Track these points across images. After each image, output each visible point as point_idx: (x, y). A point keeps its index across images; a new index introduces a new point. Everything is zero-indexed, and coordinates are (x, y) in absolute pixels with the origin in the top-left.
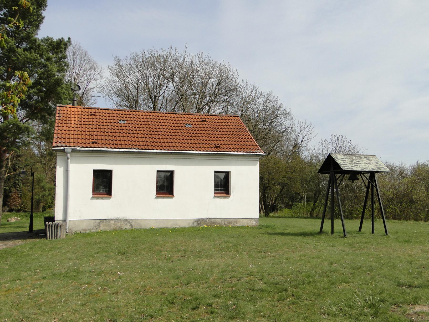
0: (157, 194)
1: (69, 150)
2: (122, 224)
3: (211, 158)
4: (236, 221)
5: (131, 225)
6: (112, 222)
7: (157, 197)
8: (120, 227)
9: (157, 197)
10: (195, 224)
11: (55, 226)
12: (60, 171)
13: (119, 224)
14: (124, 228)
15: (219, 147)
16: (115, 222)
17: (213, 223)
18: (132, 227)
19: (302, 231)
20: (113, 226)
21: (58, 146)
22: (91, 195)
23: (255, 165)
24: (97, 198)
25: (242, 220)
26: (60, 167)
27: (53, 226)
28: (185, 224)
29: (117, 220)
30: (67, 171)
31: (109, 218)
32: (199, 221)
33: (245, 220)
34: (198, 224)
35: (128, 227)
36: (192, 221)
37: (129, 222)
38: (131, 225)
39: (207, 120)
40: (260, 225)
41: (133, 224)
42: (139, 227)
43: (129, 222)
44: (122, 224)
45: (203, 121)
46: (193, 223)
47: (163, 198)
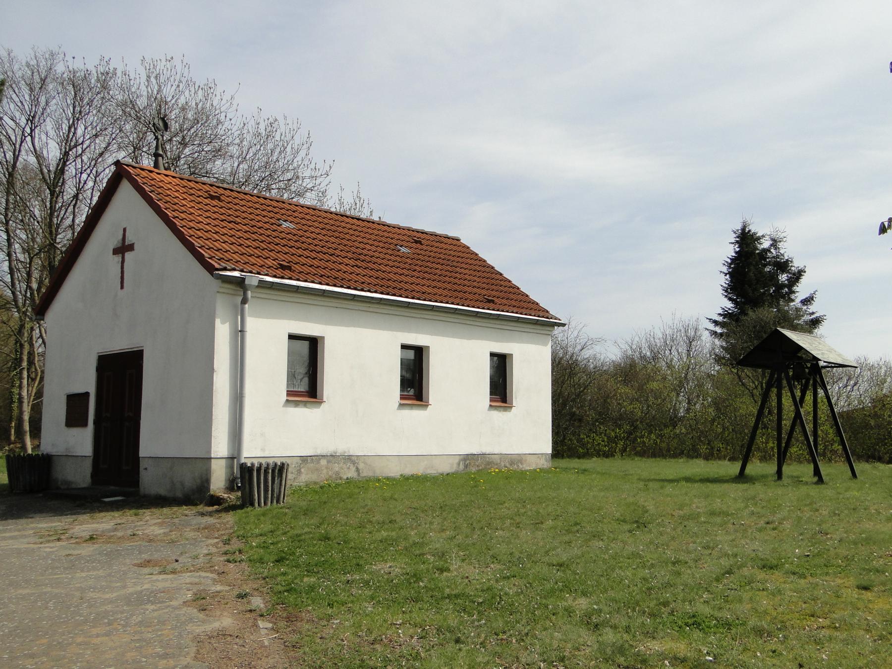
0: (401, 398)
1: (252, 280)
2: (342, 468)
3: (471, 323)
4: (519, 459)
5: (358, 470)
6: (323, 462)
7: (401, 406)
8: (337, 473)
9: (401, 406)
10: (462, 467)
11: (273, 471)
12: (222, 332)
13: (336, 467)
14: (345, 477)
15: (493, 301)
16: (328, 462)
17: (489, 463)
18: (359, 474)
19: (165, 510)
20: (325, 471)
21: (225, 269)
22: (284, 397)
23: (546, 345)
24: (296, 404)
25: (529, 457)
26: (223, 323)
27: (262, 471)
28: (446, 467)
29: (332, 457)
30: (239, 334)
31: (319, 452)
32: (468, 459)
33: (533, 458)
34: (466, 466)
35: (351, 474)
36: (457, 460)
37: (354, 463)
38: (358, 470)
39: (423, 242)
40: (315, 483)
41: (361, 466)
42: (370, 474)
43: (354, 463)
44: (342, 468)
45: (416, 242)
46: (459, 464)
47: (412, 409)
